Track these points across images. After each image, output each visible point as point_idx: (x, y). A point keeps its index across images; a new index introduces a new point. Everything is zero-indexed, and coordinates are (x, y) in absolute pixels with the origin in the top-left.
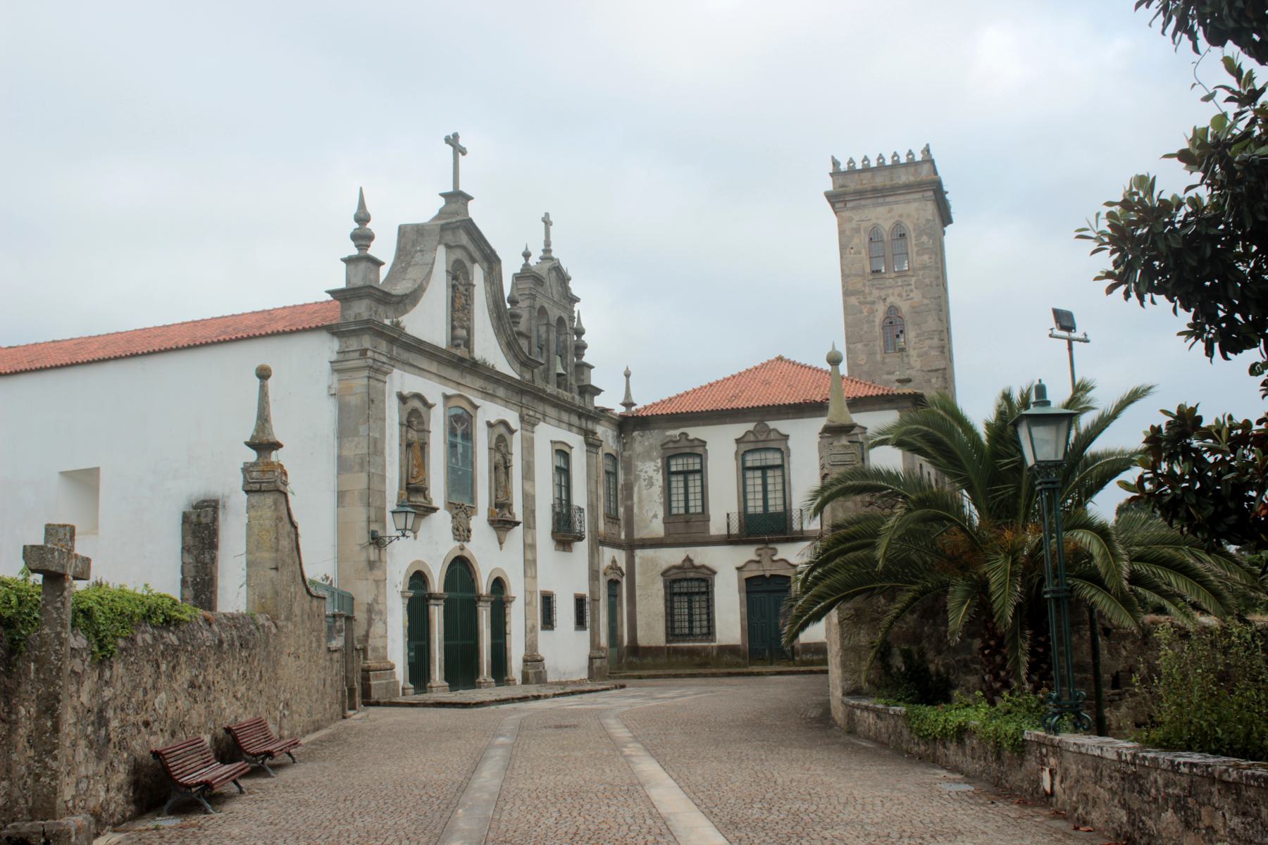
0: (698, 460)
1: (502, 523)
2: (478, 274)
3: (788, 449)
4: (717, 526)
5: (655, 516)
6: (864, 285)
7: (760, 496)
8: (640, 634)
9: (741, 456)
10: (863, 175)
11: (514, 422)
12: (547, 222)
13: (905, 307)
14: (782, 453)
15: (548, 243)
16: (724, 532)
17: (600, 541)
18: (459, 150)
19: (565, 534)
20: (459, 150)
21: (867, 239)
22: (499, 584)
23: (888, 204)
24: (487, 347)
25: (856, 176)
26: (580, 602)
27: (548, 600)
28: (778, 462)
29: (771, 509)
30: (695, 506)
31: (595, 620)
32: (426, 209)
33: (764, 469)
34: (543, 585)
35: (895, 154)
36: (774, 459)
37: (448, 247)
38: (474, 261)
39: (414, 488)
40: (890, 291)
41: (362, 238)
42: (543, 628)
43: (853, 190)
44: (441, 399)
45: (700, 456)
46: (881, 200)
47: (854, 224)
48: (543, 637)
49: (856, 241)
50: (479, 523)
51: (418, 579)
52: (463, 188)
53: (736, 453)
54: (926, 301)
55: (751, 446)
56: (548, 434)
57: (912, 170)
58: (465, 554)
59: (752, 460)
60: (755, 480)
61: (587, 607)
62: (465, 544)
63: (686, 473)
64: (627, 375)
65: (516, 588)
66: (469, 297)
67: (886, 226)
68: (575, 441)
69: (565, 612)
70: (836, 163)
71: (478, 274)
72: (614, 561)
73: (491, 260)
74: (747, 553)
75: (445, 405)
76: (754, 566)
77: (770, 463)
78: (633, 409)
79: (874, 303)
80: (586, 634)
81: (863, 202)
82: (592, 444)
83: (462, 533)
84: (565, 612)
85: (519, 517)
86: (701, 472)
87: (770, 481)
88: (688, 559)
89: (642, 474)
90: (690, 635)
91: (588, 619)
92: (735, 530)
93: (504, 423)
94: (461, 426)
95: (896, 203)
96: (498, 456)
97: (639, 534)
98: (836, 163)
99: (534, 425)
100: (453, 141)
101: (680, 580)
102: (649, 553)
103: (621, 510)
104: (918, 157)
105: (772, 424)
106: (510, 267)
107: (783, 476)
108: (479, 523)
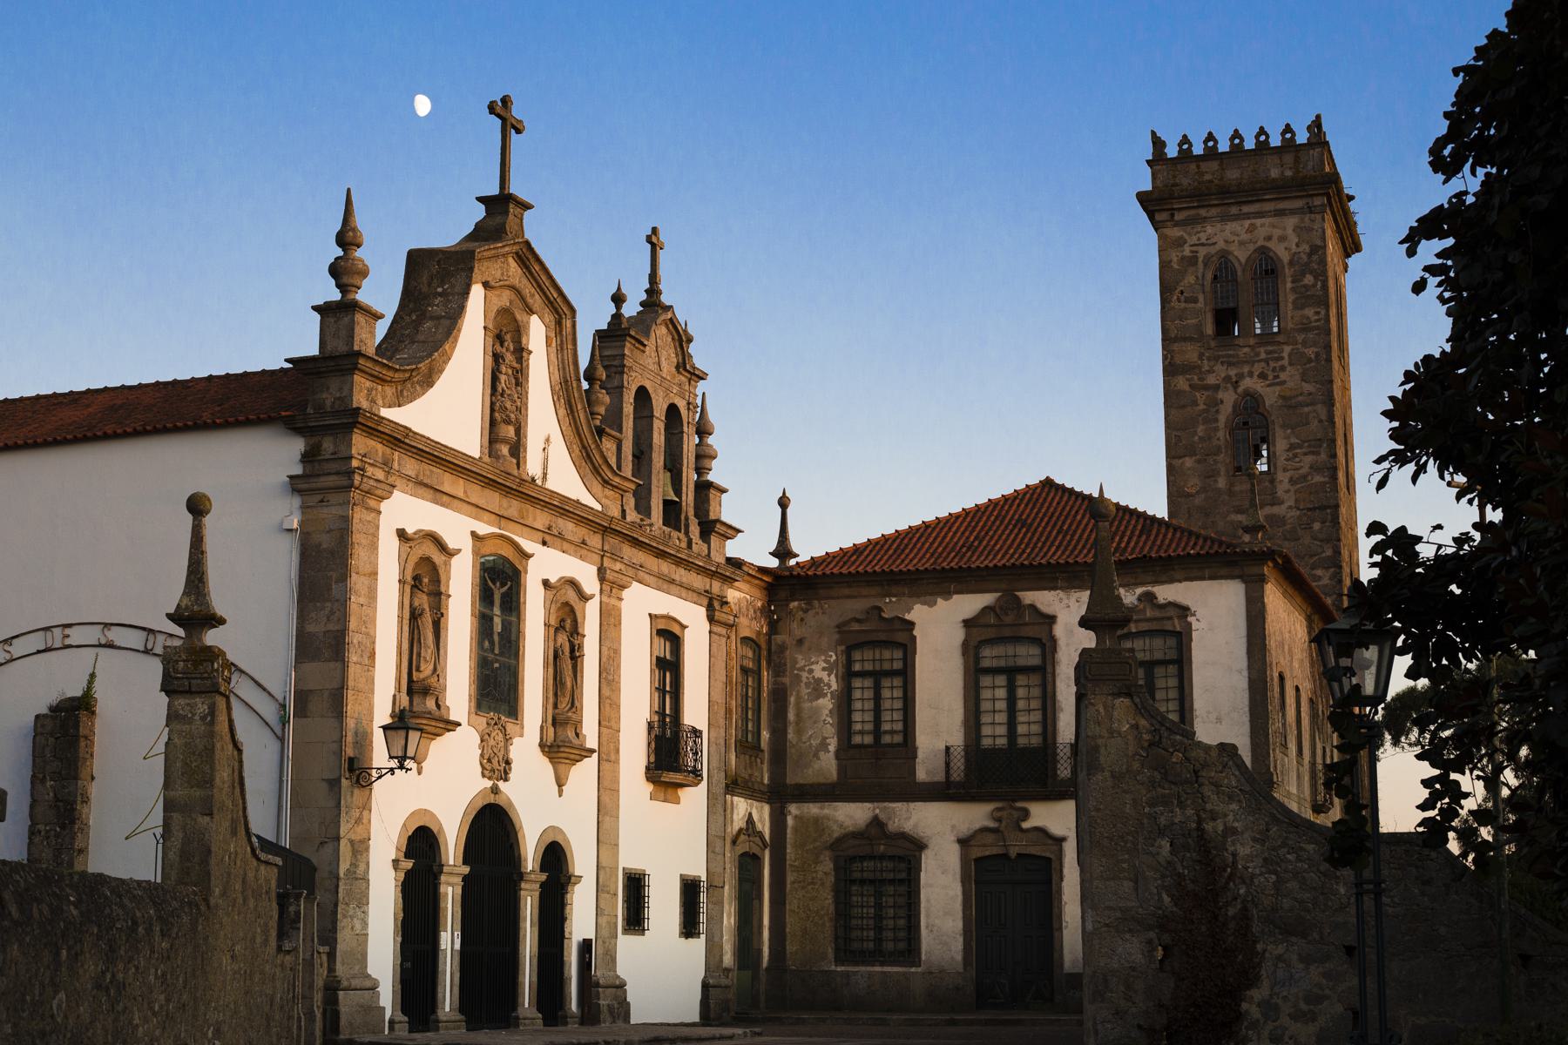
0: (898, 654)
1: (561, 747)
2: (537, 333)
3: (1054, 641)
4: (926, 768)
5: (824, 745)
6: (1201, 356)
7: (1002, 718)
8: (790, 948)
9: (971, 650)
10: (1204, 166)
11: (590, 584)
13: (1270, 396)
14: (1043, 646)
15: (653, 277)
16: (940, 777)
17: (735, 785)
18: (510, 127)
19: (669, 757)
20: (510, 127)
21: (1209, 276)
22: (555, 855)
23: (1248, 216)
24: (551, 458)
26: (690, 889)
27: (636, 885)
28: (1036, 661)
29: (1021, 741)
30: (892, 721)
31: (716, 920)
32: (449, 226)
33: (1011, 672)
34: (629, 859)
35: (1262, 131)
36: (1028, 655)
37: (486, 285)
38: (531, 311)
40: (1246, 369)
41: (347, 238)
42: (626, 931)
43: (1184, 189)
45: (903, 646)
46: (1234, 210)
47: (1187, 251)
49: (1191, 279)
50: (525, 748)
51: (421, 843)
53: (965, 645)
54: (1307, 387)
55: (990, 633)
56: (642, 603)
57: (1289, 158)
58: (500, 801)
59: (990, 657)
60: (995, 692)
61: (703, 897)
62: (501, 784)
63: (877, 676)
64: (783, 503)
65: (583, 861)
66: (520, 377)
67: (1241, 255)
69: (664, 906)
70: (1158, 144)
71: (537, 333)
72: (750, 820)
73: (561, 311)
74: (974, 816)
75: (476, 552)
76: (990, 838)
77: (1021, 662)
78: (792, 562)
79: (1216, 388)
80: (698, 945)
81: (1203, 212)
82: (714, 607)
83: (497, 766)
84: (664, 906)
85: (592, 742)
86: (906, 674)
87: (1021, 692)
88: (876, 822)
89: (805, 675)
90: (877, 955)
91: (703, 918)
92: (958, 772)
93: (573, 584)
94: (500, 581)
95: (1260, 215)
96: (563, 639)
97: (792, 779)
98: (1158, 144)
99: (623, 587)
100: (501, 109)
101: (862, 858)
102: (813, 809)
104: (1302, 137)
105: (1029, 597)
106: (592, 317)
107: (1044, 686)
108: (525, 748)
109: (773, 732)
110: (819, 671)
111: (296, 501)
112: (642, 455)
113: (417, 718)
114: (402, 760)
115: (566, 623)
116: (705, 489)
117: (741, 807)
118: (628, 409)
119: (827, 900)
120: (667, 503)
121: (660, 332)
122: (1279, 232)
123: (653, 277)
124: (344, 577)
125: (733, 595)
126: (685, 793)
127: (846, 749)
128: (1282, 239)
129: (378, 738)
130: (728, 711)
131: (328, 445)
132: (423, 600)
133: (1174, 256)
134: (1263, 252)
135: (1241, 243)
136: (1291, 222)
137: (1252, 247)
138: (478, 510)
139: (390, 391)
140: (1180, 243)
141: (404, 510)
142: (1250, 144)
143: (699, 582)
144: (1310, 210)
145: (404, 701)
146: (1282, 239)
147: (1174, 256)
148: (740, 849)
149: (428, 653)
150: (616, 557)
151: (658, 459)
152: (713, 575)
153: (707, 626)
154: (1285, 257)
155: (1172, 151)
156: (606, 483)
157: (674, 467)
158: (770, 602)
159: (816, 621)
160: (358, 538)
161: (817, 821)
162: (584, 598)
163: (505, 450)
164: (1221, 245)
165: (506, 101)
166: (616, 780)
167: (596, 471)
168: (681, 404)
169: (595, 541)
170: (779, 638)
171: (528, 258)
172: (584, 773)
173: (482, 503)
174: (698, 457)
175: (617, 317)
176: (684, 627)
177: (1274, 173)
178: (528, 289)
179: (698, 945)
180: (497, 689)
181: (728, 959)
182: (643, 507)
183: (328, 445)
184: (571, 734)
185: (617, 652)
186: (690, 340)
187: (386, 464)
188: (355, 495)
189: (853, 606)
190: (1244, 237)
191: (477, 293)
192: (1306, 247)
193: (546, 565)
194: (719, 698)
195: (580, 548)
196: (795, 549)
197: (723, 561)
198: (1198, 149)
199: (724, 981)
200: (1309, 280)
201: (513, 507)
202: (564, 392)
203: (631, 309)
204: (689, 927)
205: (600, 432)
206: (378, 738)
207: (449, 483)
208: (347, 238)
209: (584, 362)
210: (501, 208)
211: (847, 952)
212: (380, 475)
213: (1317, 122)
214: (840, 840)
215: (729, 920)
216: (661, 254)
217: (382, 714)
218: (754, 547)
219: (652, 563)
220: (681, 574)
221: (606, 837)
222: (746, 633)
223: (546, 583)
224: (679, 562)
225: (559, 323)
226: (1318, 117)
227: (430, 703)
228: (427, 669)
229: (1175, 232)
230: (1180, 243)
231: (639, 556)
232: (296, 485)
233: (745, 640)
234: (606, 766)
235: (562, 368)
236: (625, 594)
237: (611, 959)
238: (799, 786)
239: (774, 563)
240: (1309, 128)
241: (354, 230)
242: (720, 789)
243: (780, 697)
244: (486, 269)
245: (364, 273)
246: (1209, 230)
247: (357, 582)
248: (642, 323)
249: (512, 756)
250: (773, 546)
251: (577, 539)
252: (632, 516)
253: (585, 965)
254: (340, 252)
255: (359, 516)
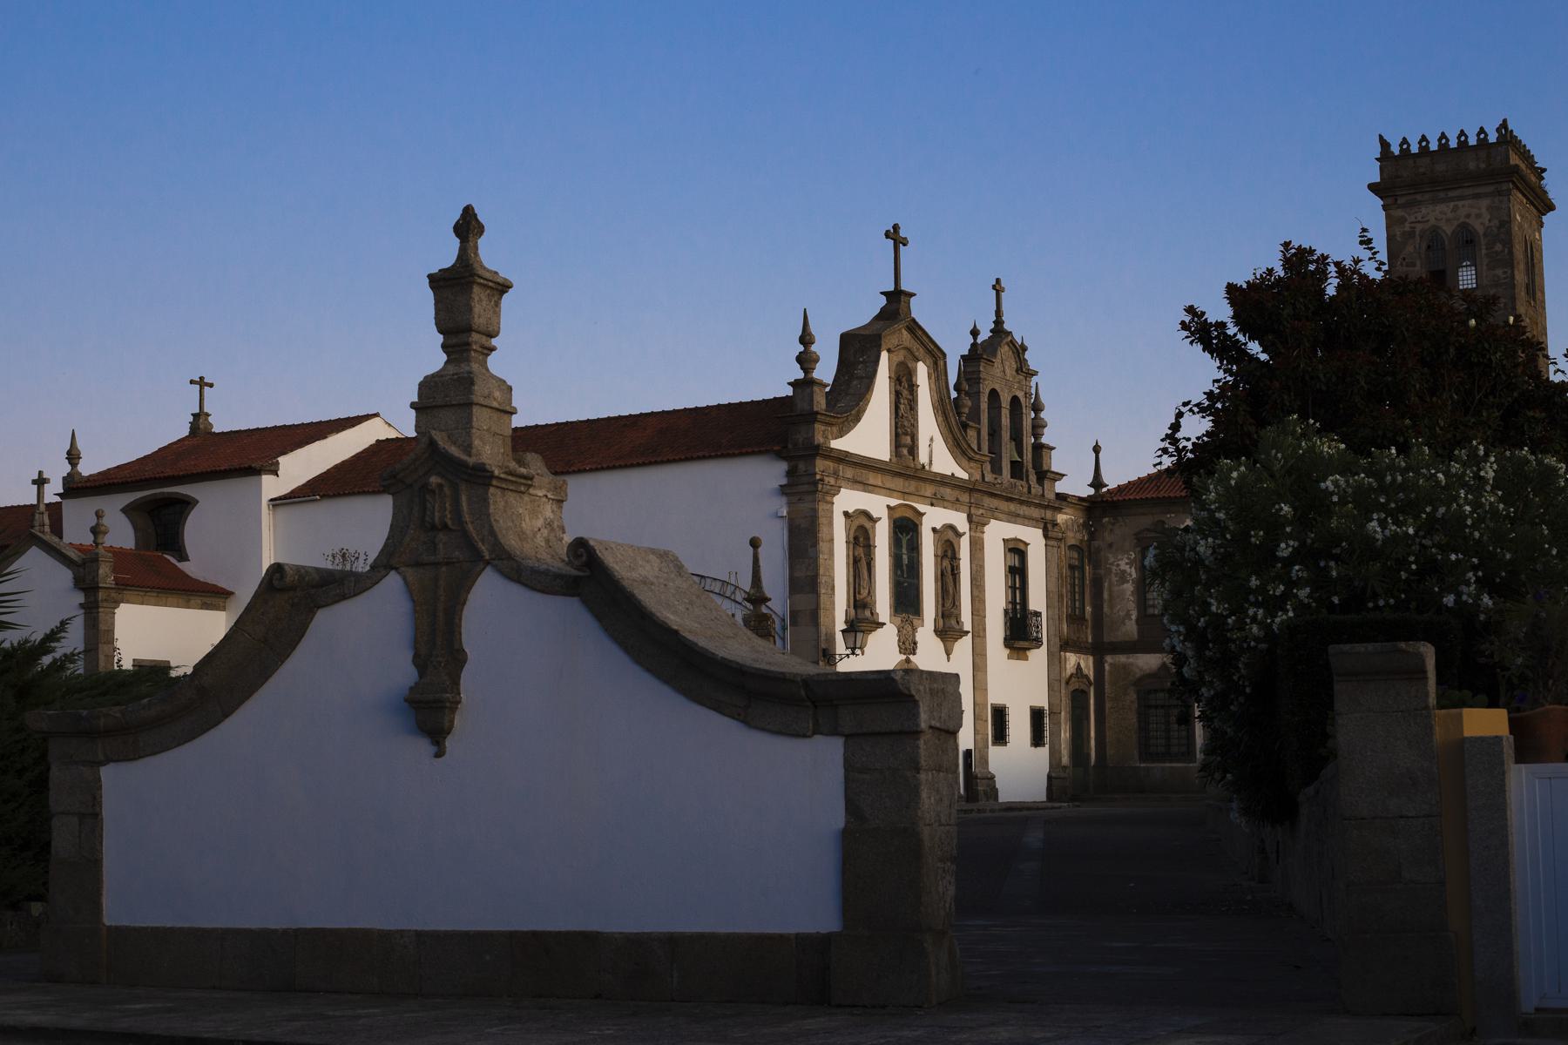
1: (948, 632)
2: (922, 372)
5: (1128, 615)
8: (1110, 752)
12: (998, 288)
15: (998, 313)
17: (1066, 645)
19: (1020, 632)
21: (1424, 246)
23: (1452, 199)
24: (936, 454)
25: (1411, 162)
26: (1037, 715)
27: (1000, 714)
31: (1055, 734)
32: (863, 311)
34: (994, 698)
37: (889, 351)
39: (861, 604)
41: (806, 339)
42: (994, 743)
44: (886, 511)
46: (1442, 195)
47: (1407, 227)
48: (994, 752)
49: (1410, 249)
52: (904, 287)
56: (997, 532)
61: (1047, 720)
64: (1097, 449)
67: (1448, 229)
68: (1034, 538)
69: (1020, 727)
70: (1384, 144)
71: (922, 372)
72: (1079, 667)
73: (936, 357)
75: (890, 517)
80: (1044, 752)
81: (1418, 197)
82: (1048, 528)
83: (908, 645)
84: (1020, 727)
85: (967, 626)
91: (1047, 734)
93: (952, 527)
94: (905, 529)
96: (946, 563)
98: (1384, 144)
100: (895, 237)
101: (1156, 691)
102: (1122, 659)
103: (1088, 609)
106: (955, 347)
109: (1094, 607)
110: (1124, 566)
111: (784, 500)
112: (994, 433)
113: (861, 624)
114: (853, 649)
115: (948, 553)
116: (1040, 449)
117: (1072, 659)
118: (984, 406)
119: (1133, 719)
120: (1013, 463)
121: (1004, 350)
122: (1476, 212)
123: (998, 313)
124: (815, 544)
125: (1061, 518)
126: (1033, 654)
127: (1143, 618)
128: (1478, 216)
129: (839, 637)
130: (1061, 596)
131: (802, 466)
132: (860, 551)
133: (1398, 231)
134: (1464, 227)
135: (1448, 220)
136: (1485, 203)
137: (1456, 223)
138: (890, 492)
139: (835, 429)
140: (1402, 220)
141: (848, 500)
142: (1453, 144)
143: (1036, 513)
144: (1500, 193)
145: (852, 611)
146: (1478, 216)
147: (1398, 231)
148: (1071, 688)
149: (865, 583)
150: (978, 506)
151: (1006, 435)
152: (1046, 507)
153: (1043, 541)
154: (1480, 230)
155: (1396, 150)
156: (970, 459)
157: (1017, 438)
158: (1089, 518)
159: (1120, 531)
160: (822, 520)
161: (1125, 667)
162: (959, 535)
163: (905, 451)
164: (1433, 221)
165: (896, 227)
166: (985, 649)
167: (964, 453)
168: (1020, 395)
169: (965, 498)
170: (1096, 543)
171: (914, 328)
172: (964, 646)
173: (892, 486)
174: (1034, 427)
175: (974, 345)
176: (1027, 544)
177: (1472, 166)
178: (915, 346)
179: (1044, 752)
180: (906, 600)
181: (1065, 760)
182: (996, 470)
183: (802, 466)
184: (953, 622)
185: (982, 567)
186: (1024, 349)
187: (836, 474)
188: (819, 495)
189: (1146, 521)
190: (1450, 215)
191: (884, 356)
192: (1496, 222)
193: (934, 517)
194: (1054, 588)
195: (955, 505)
196: (1106, 481)
197: (1052, 497)
198: (1415, 149)
199: (1062, 775)
200: (1498, 247)
201: (911, 486)
202: (942, 407)
203: (984, 335)
204: (1037, 740)
205: (965, 426)
206: (839, 637)
207: (874, 478)
208: (806, 339)
209: (952, 378)
210: (897, 299)
211: (1147, 754)
212: (832, 481)
213: (1504, 124)
214: (1140, 679)
215: (1065, 734)
216: (1003, 295)
217: (840, 625)
218: (1076, 484)
219: (1004, 505)
220: (1024, 510)
221: (980, 686)
222: (1073, 542)
223: (934, 530)
224: (1022, 502)
225: (936, 363)
226: (1505, 121)
227: (867, 613)
228: (864, 593)
229: (1399, 213)
230: (1402, 220)
231: (995, 503)
232: (783, 490)
233: (1071, 547)
234: (978, 640)
235: (939, 391)
236: (986, 528)
237: (985, 761)
238: (1111, 643)
239: (1092, 491)
240: (1498, 130)
241: (810, 334)
242: (1056, 649)
243: (1097, 584)
244: (890, 340)
245: (817, 360)
246: (1424, 211)
247: (823, 546)
248: (995, 345)
249: (917, 639)
250: (1090, 480)
251: (952, 499)
252: (989, 477)
253: (968, 765)
254: (802, 348)
255: (822, 507)
